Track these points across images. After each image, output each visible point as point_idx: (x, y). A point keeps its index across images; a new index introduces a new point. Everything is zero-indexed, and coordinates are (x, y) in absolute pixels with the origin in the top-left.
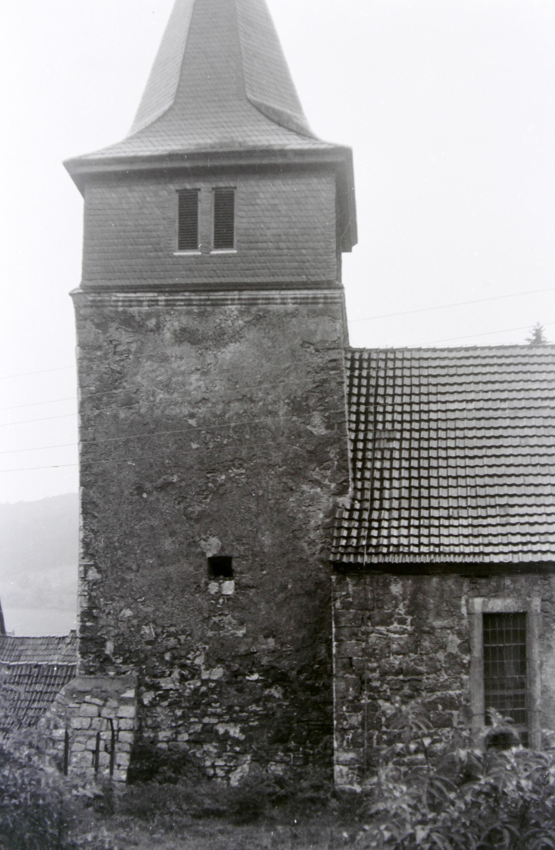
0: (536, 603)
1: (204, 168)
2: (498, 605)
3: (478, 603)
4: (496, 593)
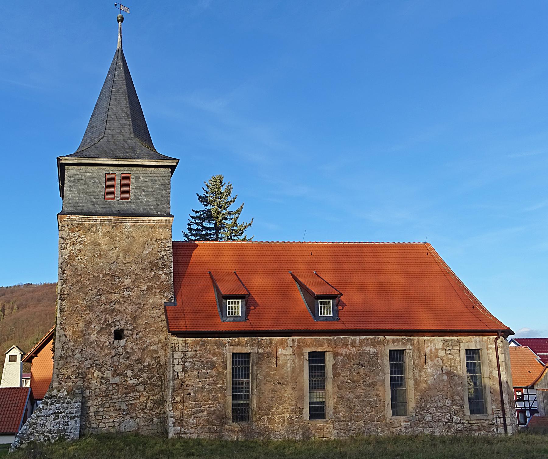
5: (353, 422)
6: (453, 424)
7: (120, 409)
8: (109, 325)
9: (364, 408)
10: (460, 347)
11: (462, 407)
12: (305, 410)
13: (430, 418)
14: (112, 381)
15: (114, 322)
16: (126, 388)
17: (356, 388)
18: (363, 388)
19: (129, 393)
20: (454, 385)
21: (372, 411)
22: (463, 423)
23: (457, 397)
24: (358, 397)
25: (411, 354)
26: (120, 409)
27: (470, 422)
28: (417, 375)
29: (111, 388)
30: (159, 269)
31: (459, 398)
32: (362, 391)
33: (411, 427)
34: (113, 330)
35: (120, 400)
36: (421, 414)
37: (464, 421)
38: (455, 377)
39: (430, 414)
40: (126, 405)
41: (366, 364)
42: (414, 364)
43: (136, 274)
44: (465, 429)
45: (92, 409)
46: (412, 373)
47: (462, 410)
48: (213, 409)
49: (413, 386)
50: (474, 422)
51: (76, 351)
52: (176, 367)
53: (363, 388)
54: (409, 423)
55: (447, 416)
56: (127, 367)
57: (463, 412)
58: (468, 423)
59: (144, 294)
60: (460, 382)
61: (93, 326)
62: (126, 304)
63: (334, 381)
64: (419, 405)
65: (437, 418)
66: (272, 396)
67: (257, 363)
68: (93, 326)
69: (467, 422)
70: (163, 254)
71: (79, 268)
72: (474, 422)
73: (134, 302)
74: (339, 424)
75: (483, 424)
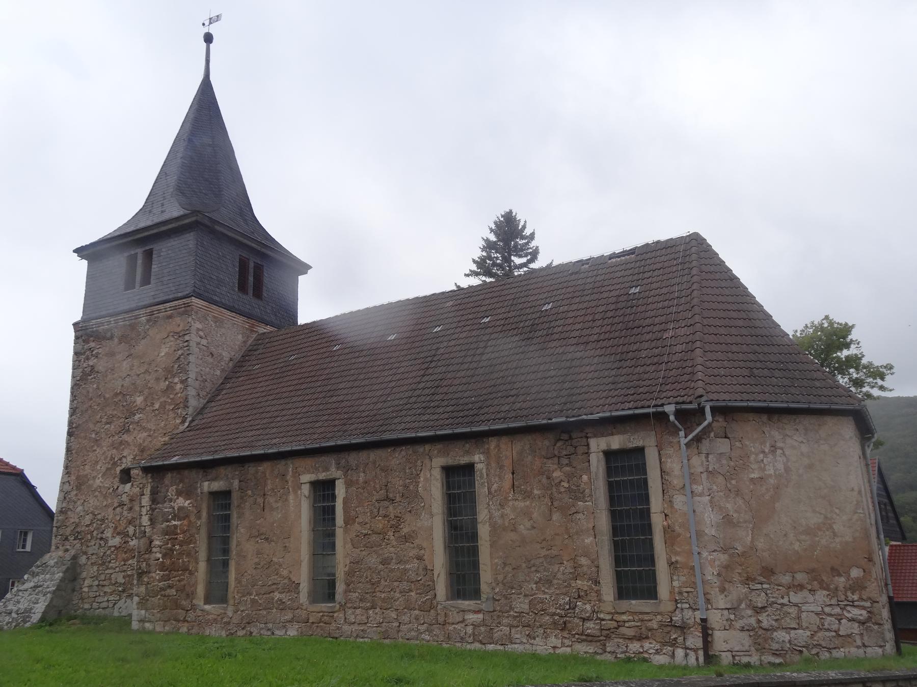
0: (236, 483)
1: (150, 235)
2: (217, 486)
3: (206, 483)
5: (378, 610)
6: (576, 620)
7: (116, 583)
8: (115, 464)
9: (396, 584)
10: (589, 448)
11: (597, 582)
12: (301, 586)
13: (526, 607)
14: (111, 543)
15: (120, 459)
16: (126, 553)
17: (380, 545)
18: (395, 543)
19: (128, 560)
20: (577, 533)
21: (410, 590)
22: (598, 618)
23: (584, 561)
24: (385, 562)
25: (484, 471)
26: (116, 583)
27: (617, 617)
28: (497, 514)
29: (109, 552)
30: (174, 376)
31: (589, 562)
32: (392, 549)
33: (483, 623)
34: (118, 469)
35: (117, 569)
36: (506, 598)
37: (602, 616)
38: (580, 516)
39: (526, 596)
40: (124, 577)
41: (398, 499)
42: (490, 493)
43: (150, 388)
44: (605, 633)
45: (87, 582)
46: (486, 511)
47: (596, 588)
48: (182, 583)
49: (488, 539)
50: (624, 617)
51: (79, 503)
52: (143, 517)
53: (395, 543)
54: (480, 616)
55: (562, 602)
56: (130, 522)
57: (598, 593)
58: (612, 620)
59: (155, 416)
60: (591, 526)
61: (98, 468)
62: (136, 432)
63: (346, 530)
64: (500, 577)
65: (539, 607)
66: (257, 560)
67: (238, 506)
68: (98, 468)
69: (608, 617)
70: (180, 352)
71: (91, 390)
72: (624, 617)
73: (144, 428)
74: (353, 613)
75: (649, 624)
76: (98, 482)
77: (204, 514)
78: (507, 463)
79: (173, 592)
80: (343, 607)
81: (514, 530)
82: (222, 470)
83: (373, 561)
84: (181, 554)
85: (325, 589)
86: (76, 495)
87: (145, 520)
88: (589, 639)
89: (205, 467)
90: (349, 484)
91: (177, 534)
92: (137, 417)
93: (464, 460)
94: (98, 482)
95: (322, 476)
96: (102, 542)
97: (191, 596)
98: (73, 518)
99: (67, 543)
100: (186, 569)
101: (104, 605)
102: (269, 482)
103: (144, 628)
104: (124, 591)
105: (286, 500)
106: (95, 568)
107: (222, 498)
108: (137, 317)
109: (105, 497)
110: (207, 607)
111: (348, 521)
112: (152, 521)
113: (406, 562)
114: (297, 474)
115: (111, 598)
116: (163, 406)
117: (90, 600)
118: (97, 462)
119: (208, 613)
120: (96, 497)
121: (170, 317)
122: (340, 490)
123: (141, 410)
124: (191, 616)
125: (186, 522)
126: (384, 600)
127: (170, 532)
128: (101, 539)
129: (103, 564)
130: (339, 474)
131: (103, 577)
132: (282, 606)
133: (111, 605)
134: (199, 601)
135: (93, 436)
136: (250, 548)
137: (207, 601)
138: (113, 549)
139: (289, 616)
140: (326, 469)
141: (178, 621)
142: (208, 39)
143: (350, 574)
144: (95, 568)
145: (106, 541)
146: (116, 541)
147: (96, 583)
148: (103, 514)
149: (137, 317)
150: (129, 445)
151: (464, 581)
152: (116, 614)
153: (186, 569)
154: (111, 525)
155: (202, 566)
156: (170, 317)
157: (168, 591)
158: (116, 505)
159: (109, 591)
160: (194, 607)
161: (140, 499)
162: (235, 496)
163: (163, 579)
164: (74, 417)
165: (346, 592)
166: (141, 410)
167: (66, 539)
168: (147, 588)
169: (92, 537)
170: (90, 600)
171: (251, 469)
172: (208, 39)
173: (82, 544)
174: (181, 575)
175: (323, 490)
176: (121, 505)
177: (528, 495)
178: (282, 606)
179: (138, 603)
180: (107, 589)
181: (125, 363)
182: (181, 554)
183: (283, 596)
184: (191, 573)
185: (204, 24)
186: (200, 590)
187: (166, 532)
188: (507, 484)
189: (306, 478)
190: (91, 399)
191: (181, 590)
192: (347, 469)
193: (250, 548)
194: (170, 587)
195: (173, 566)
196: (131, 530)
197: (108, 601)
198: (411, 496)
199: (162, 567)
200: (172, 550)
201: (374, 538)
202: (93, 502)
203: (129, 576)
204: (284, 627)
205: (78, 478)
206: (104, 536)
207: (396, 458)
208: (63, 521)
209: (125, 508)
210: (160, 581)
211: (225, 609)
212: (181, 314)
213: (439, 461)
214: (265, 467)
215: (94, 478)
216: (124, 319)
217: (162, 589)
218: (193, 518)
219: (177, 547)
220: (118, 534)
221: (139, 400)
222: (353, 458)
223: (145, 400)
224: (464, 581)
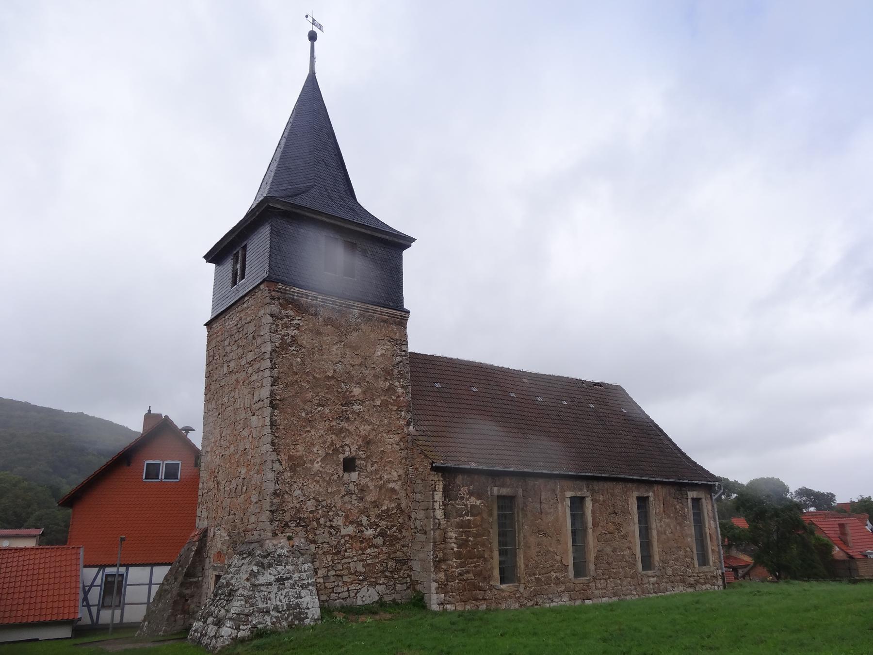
0: (520, 491)
1: (343, 227)
2: (505, 491)
3: (496, 489)
4: (503, 485)
8: (336, 451)
11: (692, 559)
15: (342, 447)
19: (365, 549)
34: (341, 457)
48: (479, 569)
59: (377, 411)
63: (594, 531)
66: (538, 550)
71: (294, 364)
76: (317, 466)
77: (495, 513)
78: (661, 498)
79: (471, 576)
80: (595, 579)
81: (665, 533)
82: (508, 480)
83: (608, 549)
84: (475, 545)
85: (580, 569)
86: (291, 477)
87: (439, 514)
88: (691, 585)
89: (495, 476)
90: (594, 501)
91: (471, 528)
92: (356, 407)
93: (646, 495)
94: (317, 466)
95: (579, 494)
96: (332, 531)
97: (487, 578)
98: (292, 503)
99: (287, 530)
100: (481, 557)
101: (346, 594)
102: (543, 493)
103: (445, 610)
104: (365, 579)
105: (556, 508)
106: (329, 558)
107: (506, 503)
108: (349, 307)
109: (329, 483)
110: (503, 586)
111: (595, 525)
112: (447, 516)
113: (623, 551)
114: (563, 491)
115: (352, 587)
116: (384, 404)
117: (327, 592)
118: (313, 445)
119: (503, 591)
120: (317, 482)
121: (385, 321)
122: (589, 504)
123: (357, 401)
124: (489, 594)
125: (478, 518)
126: (615, 573)
127: (464, 526)
128: (331, 527)
129: (339, 553)
130: (588, 494)
131: (340, 566)
132: (557, 581)
133: (352, 595)
134: (496, 582)
135: (304, 414)
136: (533, 540)
137: (503, 581)
138: (347, 538)
139: (563, 588)
140: (581, 490)
141: (476, 600)
142: (313, 37)
143: (597, 558)
144: (329, 558)
145: (337, 529)
146: (350, 530)
147: (332, 573)
148: (329, 501)
149: (349, 307)
150: (350, 433)
151: (647, 561)
152: (359, 602)
153: (481, 557)
154: (340, 513)
155: (496, 554)
156: (385, 321)
157: (465, 576)
158: (343, 493)
159: (349, 580)
160: (491, 587)
161: (433, 495)
162: (520, 501)
163: (461, 565)
164: (276, 387)
165: (596, 569)
166: (357, 401)
167: (286, 525)
168: (446, 575)
169: (319, 524)
170: (327, 592)
171: (531, 482)
172: (313, 37)
173: (307, 531)
174: (477, 562)
175: (577, 503)
176: (349, 493)
177: (669, 517)
178: (557, 581)
179: (437, 589)
180: (346, 579)
181: (335, 347)
182: (475, 545)
183: (557, 574)
184: (485, 560)
185: (307, 16)
186: (496, 573)
187: (460, 525)
188: (662, 510)
189: (569, 494)
190: (296, 373)
191: (478, 574)
192: (593, 491)
193: (533, 540)
194: (468, 572)
195: (466, 554)
196: (364, 520)
197: (348, 591)
198: (626, 512)
199: (459, 555)
200: (467, 541)
201: (609, 536)
202: (313, 488)
203: (369, 565)
204: (560, 596)
205: (291, 458)
206: (334, 524)
207: (618, 488)
208: (280, 505)
209: (354, 496)
210: (457, 568)
211: (518, 587)
212: (395, 323)
213: (636, 494)
214: (540, 482)
215: (312, 462)
216: (334, 303)
217: (460, 574)
218: (485, 516)
219: (472, 539)
220: (351, 522)
221: (357, 391)
222: (596, 485)
223: (364, 392)
224: (647, 561)
